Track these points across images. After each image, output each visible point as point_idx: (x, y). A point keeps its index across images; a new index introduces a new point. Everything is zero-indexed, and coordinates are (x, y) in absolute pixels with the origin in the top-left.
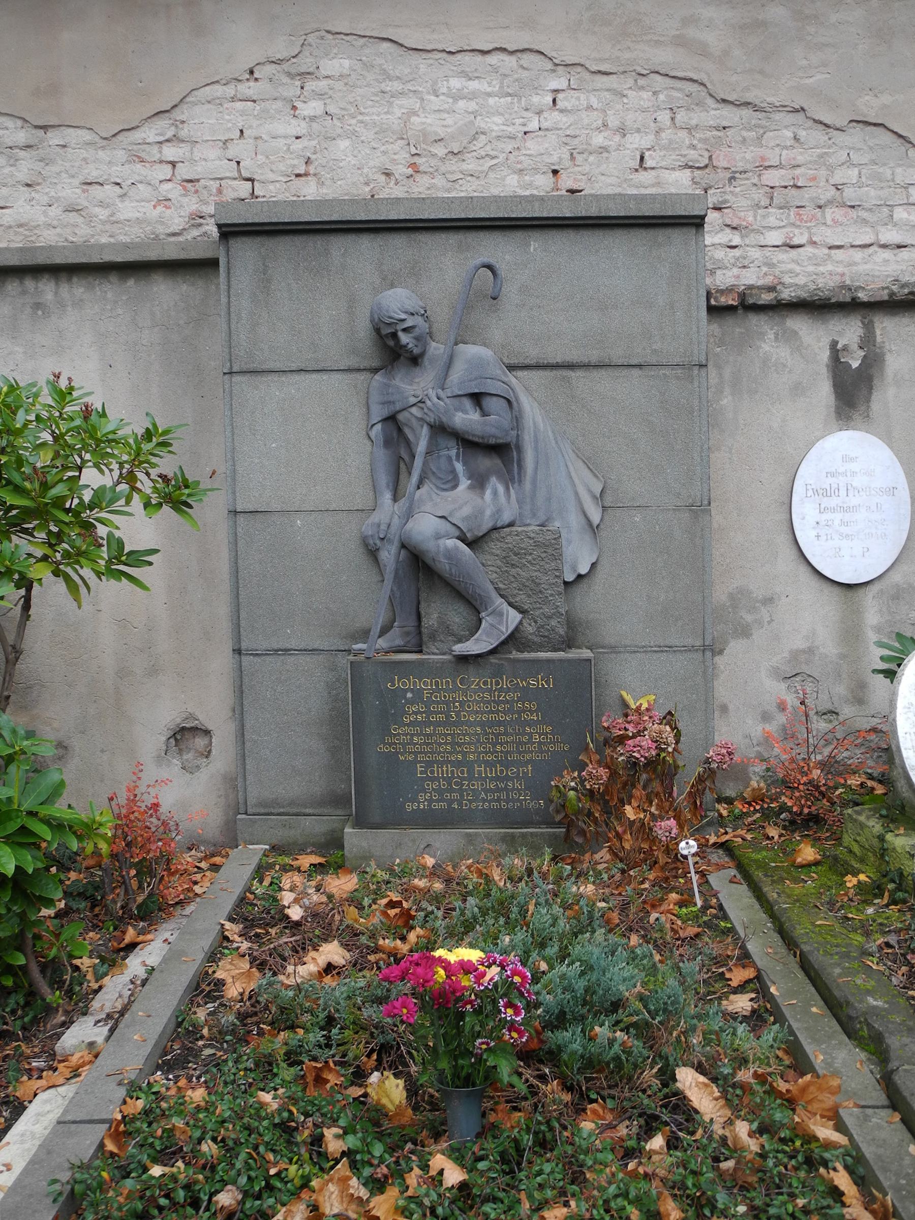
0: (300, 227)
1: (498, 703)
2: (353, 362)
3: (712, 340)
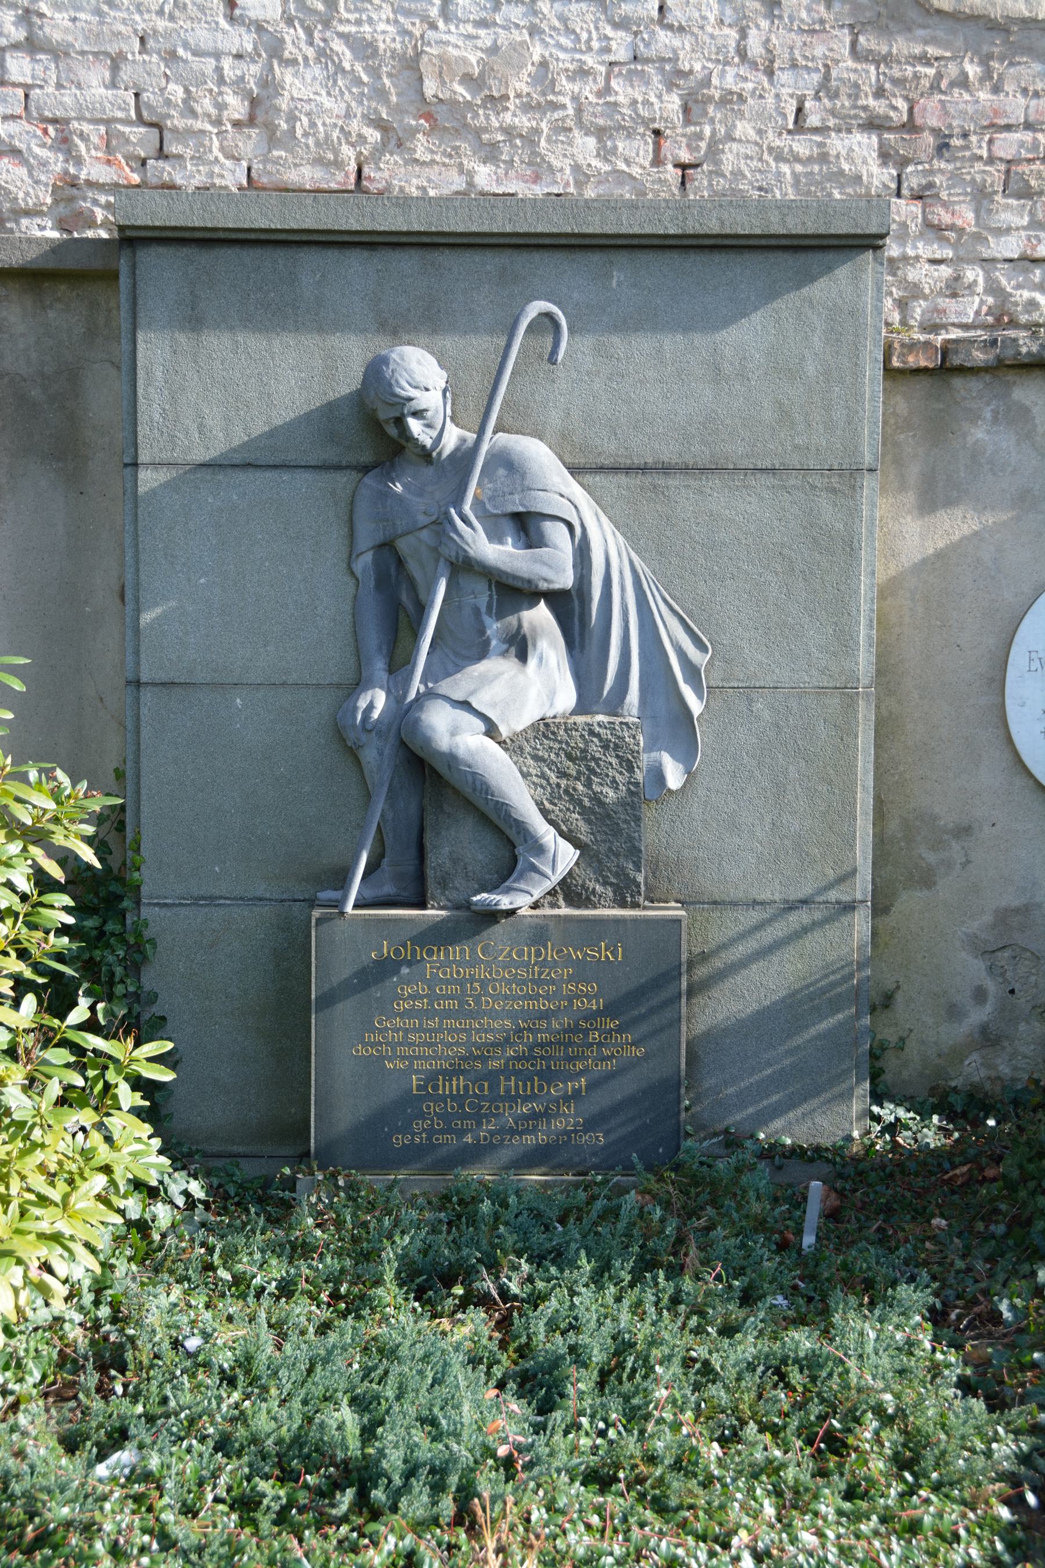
0: (253, 236)
1: (538, 982)
2: (330, 454)
3: (892, 421)
